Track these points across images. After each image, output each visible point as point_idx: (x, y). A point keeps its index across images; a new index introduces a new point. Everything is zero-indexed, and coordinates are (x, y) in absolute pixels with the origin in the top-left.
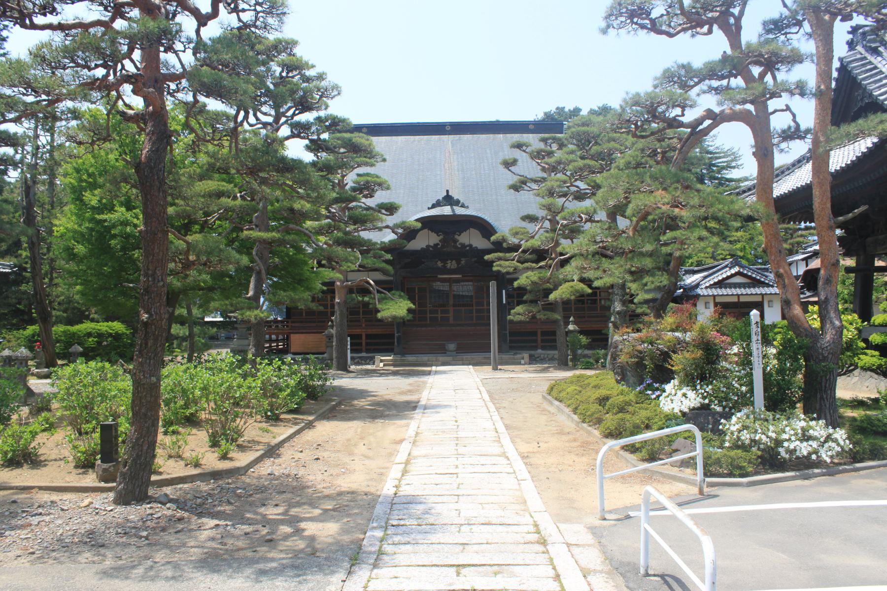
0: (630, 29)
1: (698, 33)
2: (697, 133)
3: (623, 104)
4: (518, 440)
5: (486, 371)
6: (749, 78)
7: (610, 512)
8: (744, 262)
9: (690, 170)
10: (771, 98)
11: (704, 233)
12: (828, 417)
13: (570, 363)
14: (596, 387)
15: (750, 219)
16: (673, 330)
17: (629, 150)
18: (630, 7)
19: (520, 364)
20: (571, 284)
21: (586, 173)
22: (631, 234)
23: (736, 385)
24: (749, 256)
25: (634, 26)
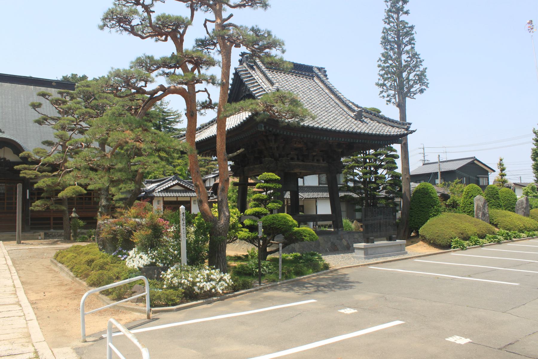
0: (118, 29)
1: (159, 39)
2: (153, 98)
3: (109, 75)
4: (30, 292)
5: (13, 245)
6: (185, 70)
7: (90, 336)
8: (181, 178)
9: (151, 121)
10: (196, 83)
11: (157, 159)
12: (222, 267)
13: (72, 238)
14: (87, 253)
15: (183, 153)
16: (135, 218)
17: (115, 105)
18: (119, 16)
19: (38, 239)
20: (73, 187)
21: (87, 117)
22: (109, 157)
23: (171, 250)
24: (185, 174)
25: (121, 28)
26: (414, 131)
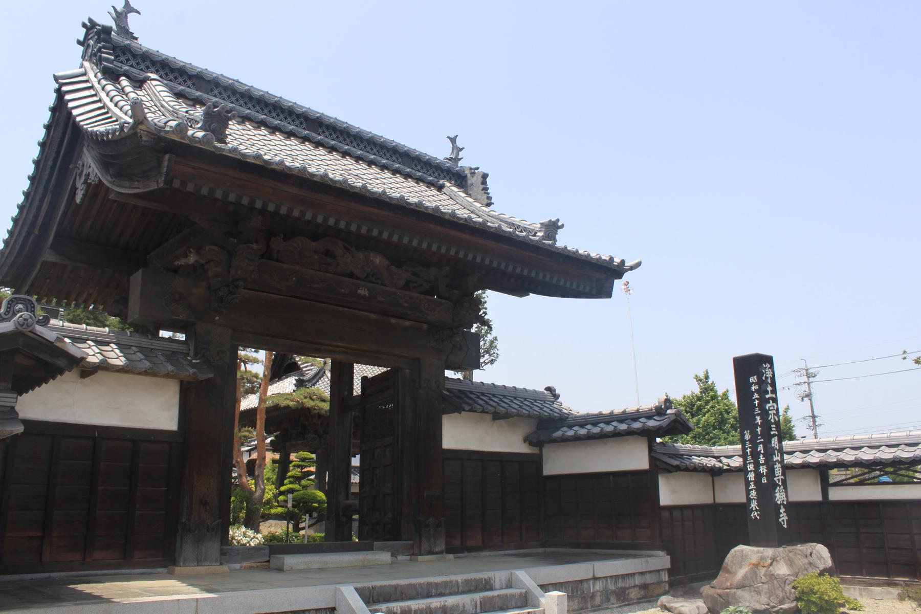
26: (639, 264)
